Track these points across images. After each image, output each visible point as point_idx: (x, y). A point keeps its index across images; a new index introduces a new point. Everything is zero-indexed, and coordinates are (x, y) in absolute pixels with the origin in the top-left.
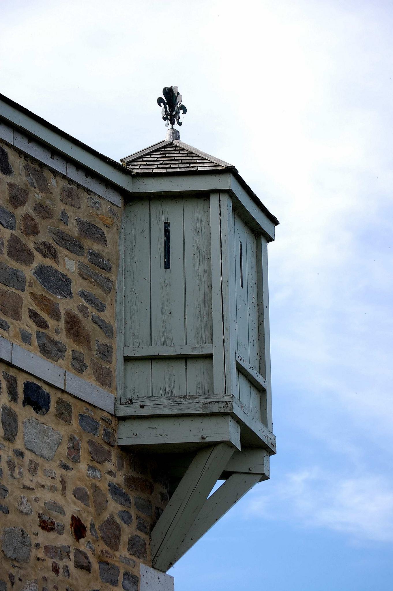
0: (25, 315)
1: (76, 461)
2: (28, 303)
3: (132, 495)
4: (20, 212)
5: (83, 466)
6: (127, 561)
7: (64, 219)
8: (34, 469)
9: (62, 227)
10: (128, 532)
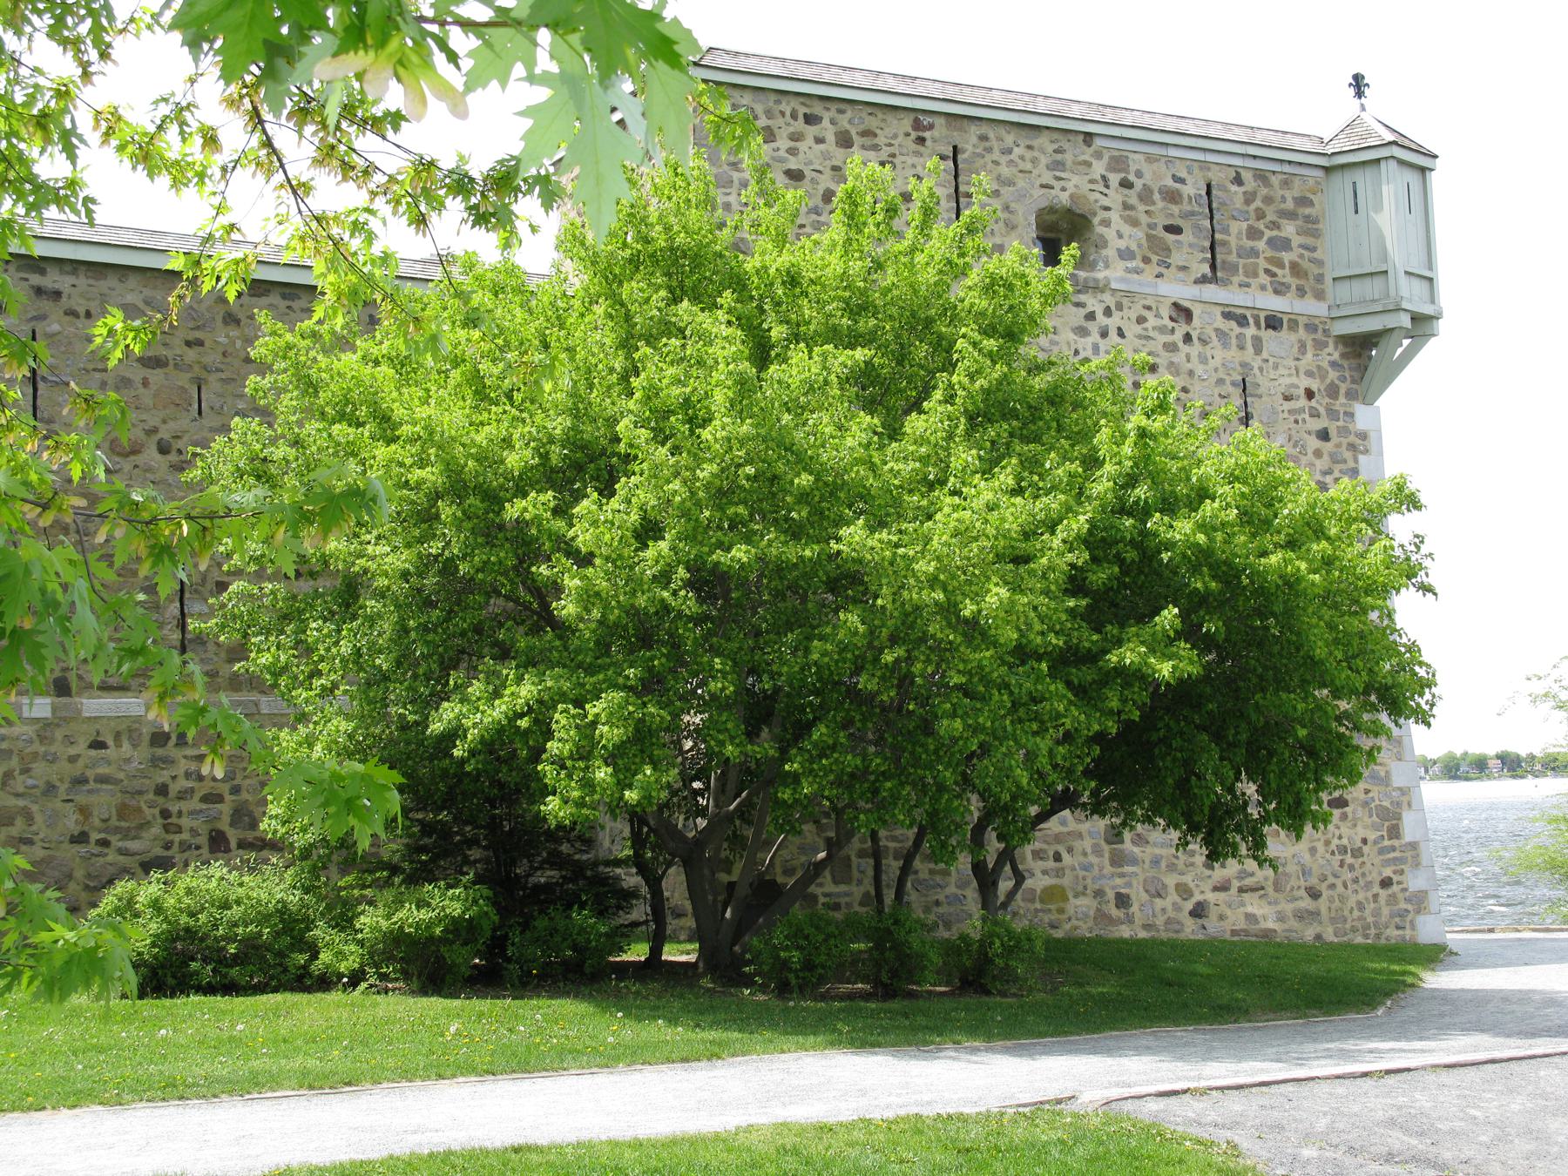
0: (1261, 273)
1: (1304, 354)
2: (1262, 264)
3: (1346, 364)
4: (1253, 206)
5: (1309, 355)
7: (1284, 199)
8: (1276, 367)
9: (1283, 206)
10: (1343, 388)
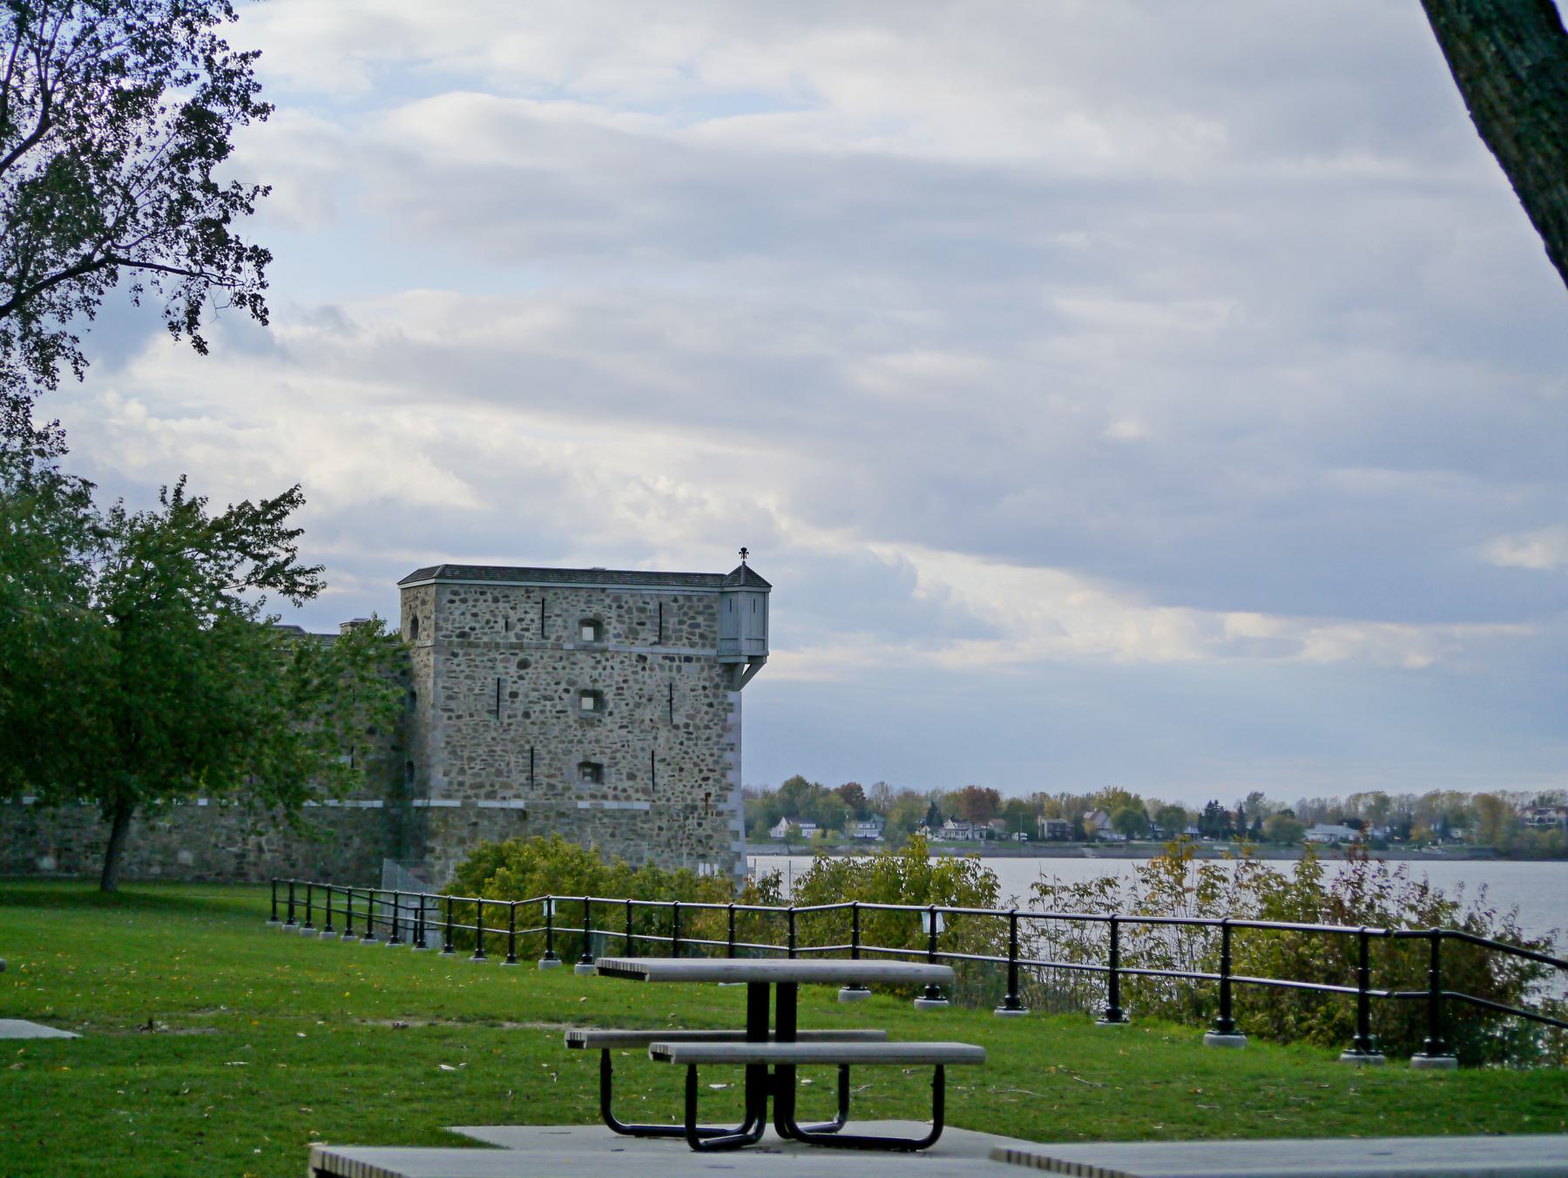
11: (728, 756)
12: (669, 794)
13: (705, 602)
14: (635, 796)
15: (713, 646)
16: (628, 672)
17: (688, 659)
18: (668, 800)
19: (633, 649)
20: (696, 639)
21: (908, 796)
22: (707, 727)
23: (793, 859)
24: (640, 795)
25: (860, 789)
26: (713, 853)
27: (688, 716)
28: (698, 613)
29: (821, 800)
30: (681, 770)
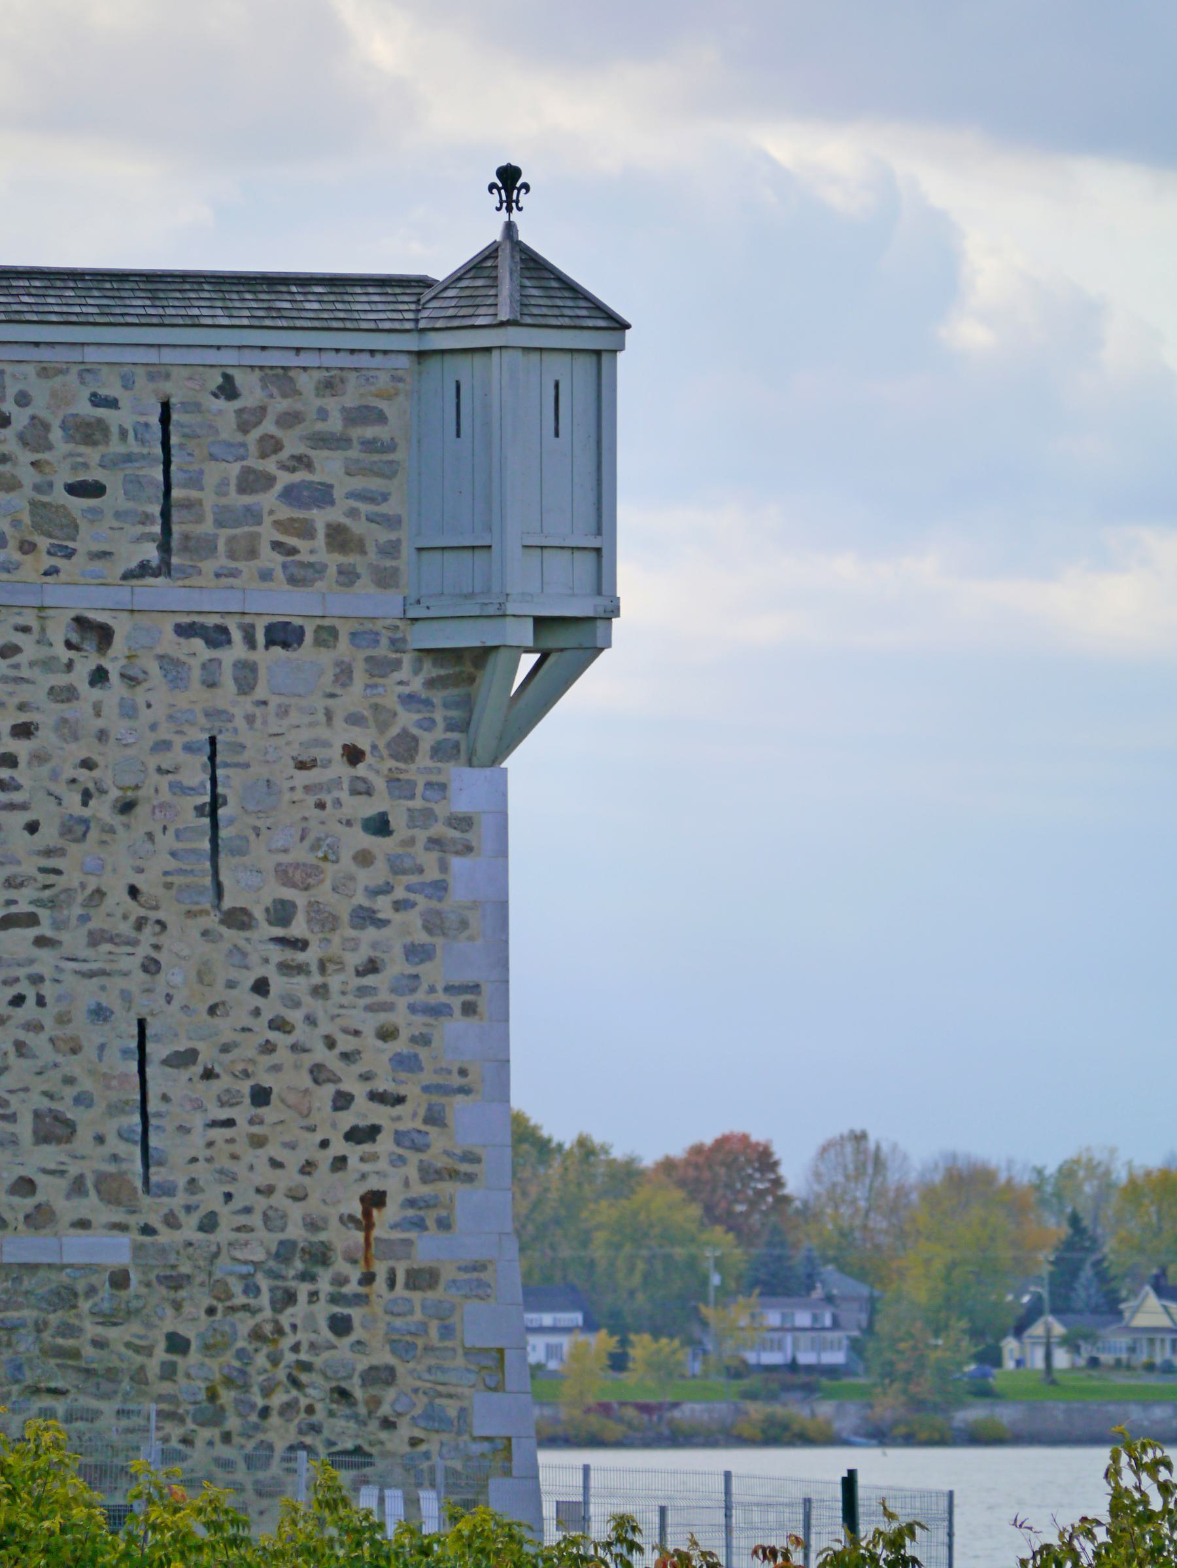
6: (429, 770)
7: (323, 414)
8: (283, 712)
9: (320, 426)
11: (455, 1032)
12: (211, 1199)
13: (351, 398)
14: (67, 1209)
15: (386, 579)
16: (37, 694)
17: (283, 636)
18: (209, 1224)
19: (54, 594)
20: (315, 550)
21: (967, 1183)
22: (365, 917)
23: (597, 1458)
24: (89, 1205)
25: (765, 1160)
26: (397, 1441)
27: (284, 874)
28: (323, 441)
29: (604, 1212)
30: (261, 1096)
